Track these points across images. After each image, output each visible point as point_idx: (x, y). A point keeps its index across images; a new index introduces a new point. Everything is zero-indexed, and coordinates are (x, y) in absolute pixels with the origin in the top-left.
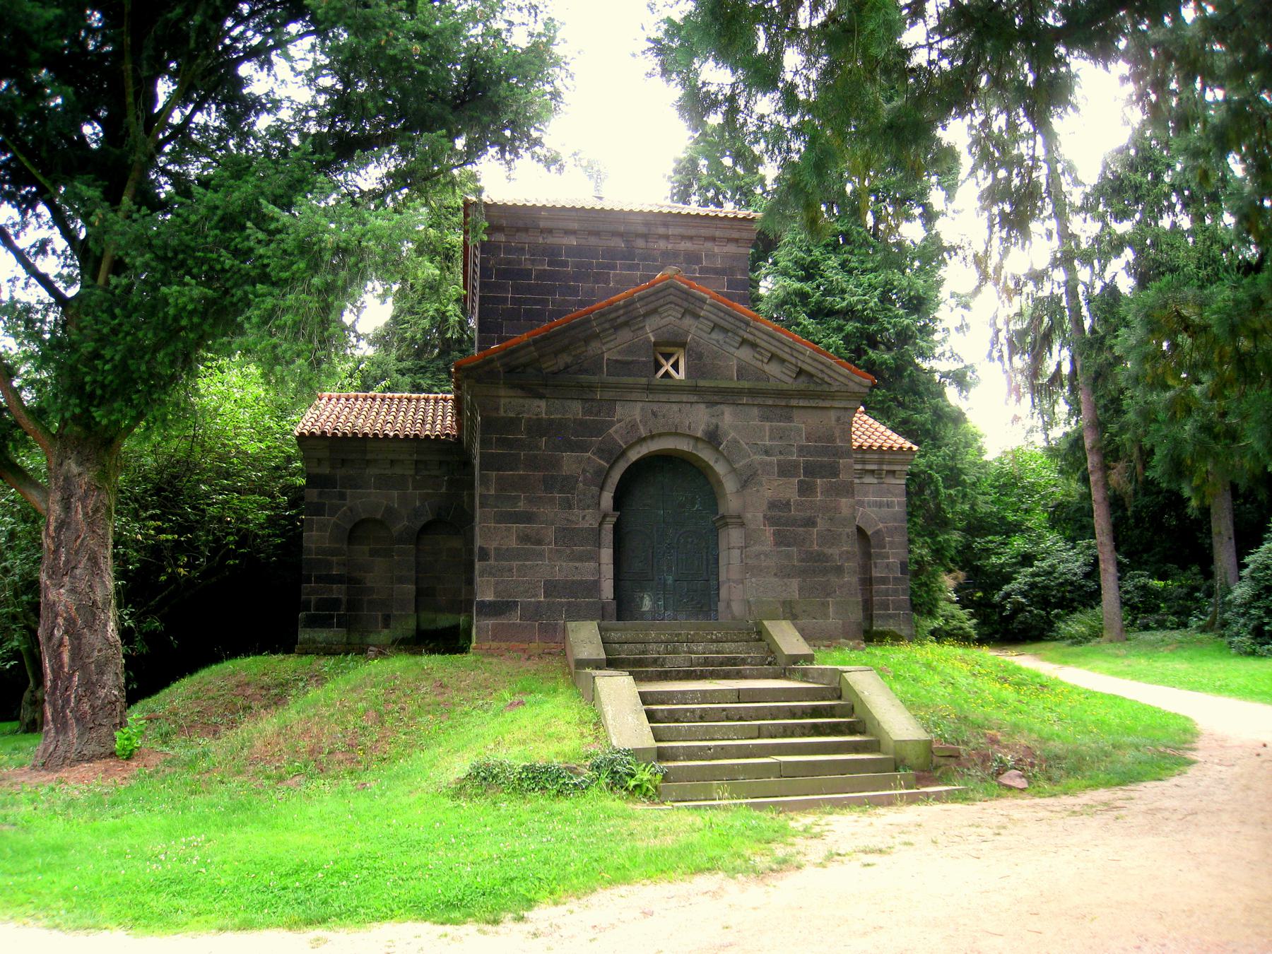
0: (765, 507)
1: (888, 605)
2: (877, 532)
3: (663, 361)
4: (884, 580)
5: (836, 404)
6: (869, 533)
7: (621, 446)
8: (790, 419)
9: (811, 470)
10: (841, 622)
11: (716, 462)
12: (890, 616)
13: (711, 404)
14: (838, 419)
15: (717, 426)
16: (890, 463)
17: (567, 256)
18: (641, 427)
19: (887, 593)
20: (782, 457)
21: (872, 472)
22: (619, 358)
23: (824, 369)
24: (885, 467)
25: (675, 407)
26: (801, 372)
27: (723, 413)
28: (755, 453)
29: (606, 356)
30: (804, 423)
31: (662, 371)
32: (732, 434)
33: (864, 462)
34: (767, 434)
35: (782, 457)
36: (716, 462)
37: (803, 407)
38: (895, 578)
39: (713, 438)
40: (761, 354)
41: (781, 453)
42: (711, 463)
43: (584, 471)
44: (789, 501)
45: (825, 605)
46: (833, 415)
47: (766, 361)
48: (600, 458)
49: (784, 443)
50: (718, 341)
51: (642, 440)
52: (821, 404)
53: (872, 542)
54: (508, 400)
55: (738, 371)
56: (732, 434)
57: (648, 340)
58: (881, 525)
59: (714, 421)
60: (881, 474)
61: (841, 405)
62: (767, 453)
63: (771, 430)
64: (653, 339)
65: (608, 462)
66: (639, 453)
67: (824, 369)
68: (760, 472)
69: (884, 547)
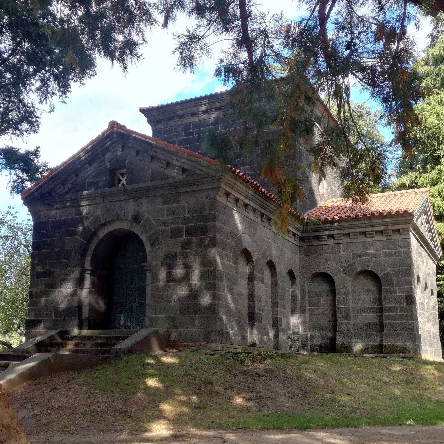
0: (162, 258)
1: (396, 327)
2: (387, 275)
3: (121, 178)
4: (391, 309)
5: (206, 187)
6: (380, 275)
7: (92, 230)
8: (179, 201)
9: (190, 232)
10: (203, 330)
11: (142, 233)
12: (397, 336)
13: (136, 199)
14: (207, 197)
15: (139, 212)
16: (394, 224)
17: (193, 129)
18: (101, 219)
19: (395, 318)
20: (173, 226)
21: (381, 232)
22: (93, 180)
23: (196, 165)
24: (390, 228)
25: (118, 204)
26: (184, 171)
27: (142, 204)
28: (158, 226)
29: (87, 180)
30: (187, 202)
31: (121, 184)
32: (147, 215)
33: (372, 226)
34: (166, 213)
35: (173, 226)
36: (142, 233)
37: (187, 192)
38: (401, 308)
39: (136, 219)
40: (162, 163)
41: (173, 223)
42: (139, 235)
43: (75, 247)
44: (177, 253)
45: (193, 319)
46: (204, 194)
47: (165, 167)
48: (82, 238)
49: (174, 217)
50: (141, 160)
51: (104, 225)
52: (196, 188)
53: (382, 282)
54: (44, 212)
55: (151, 176)
56: (147, 215)
57: (106, 167)
58: (389, 270)
59: (137, 208)
60: (388, 233)
61: (209, 187)
62: (165, 224)
63: (168, 210)
64: (109, 166)
65: (85, 240)
66: (103, 233)
67: (196, 165)
68: (161, 236)
69: (393, 285)
